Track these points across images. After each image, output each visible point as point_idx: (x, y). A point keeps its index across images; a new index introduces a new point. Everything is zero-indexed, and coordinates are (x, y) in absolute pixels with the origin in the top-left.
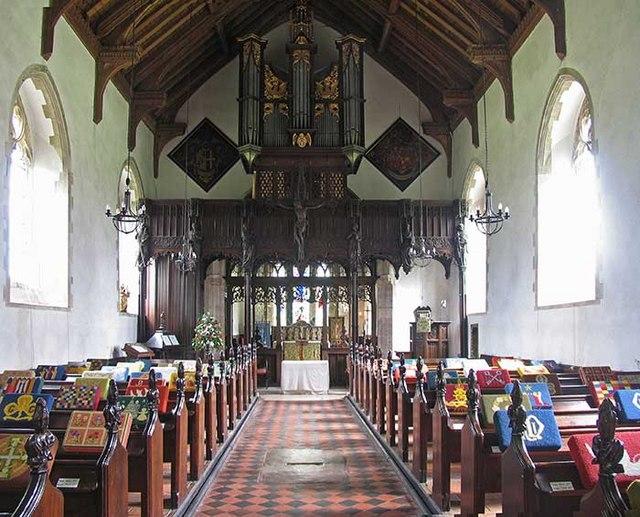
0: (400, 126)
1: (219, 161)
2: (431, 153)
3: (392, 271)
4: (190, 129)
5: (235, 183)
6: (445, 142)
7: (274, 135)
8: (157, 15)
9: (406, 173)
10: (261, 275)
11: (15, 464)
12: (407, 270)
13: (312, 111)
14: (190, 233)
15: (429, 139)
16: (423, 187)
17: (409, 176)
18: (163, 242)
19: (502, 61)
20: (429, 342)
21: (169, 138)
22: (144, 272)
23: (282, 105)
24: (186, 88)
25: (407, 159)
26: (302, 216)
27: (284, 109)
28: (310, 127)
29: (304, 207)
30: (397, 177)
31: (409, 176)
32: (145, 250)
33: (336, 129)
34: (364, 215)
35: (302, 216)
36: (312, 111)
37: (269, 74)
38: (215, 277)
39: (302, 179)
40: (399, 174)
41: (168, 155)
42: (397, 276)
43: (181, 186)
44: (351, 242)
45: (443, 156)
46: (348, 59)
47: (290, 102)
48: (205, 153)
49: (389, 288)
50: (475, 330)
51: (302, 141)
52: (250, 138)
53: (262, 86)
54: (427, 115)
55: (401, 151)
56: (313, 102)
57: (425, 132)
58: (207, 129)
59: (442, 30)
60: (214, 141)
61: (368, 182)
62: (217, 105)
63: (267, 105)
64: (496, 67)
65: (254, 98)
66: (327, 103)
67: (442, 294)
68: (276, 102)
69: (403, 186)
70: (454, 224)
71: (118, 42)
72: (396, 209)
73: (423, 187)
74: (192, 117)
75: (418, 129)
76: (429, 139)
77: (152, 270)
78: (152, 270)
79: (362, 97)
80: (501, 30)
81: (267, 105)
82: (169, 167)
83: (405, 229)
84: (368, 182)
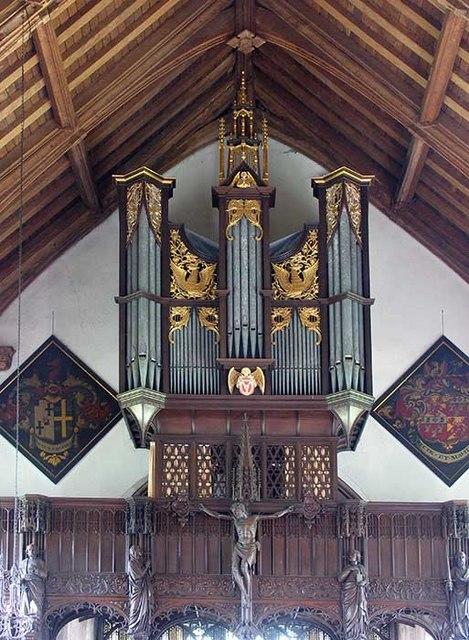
5: (114, 467)
7: (191, 368)
14: (22, 564)
26: (247, 532)
28: (261, 354)
30: (436, 455)
33: (315, 360)
35: (247, 532)
36: (266, 322)
46: (338, 218)
51: (247, 382)
53: (166, 274)
56: (267, 305)
58: (56, 360)
60: (71, 382)
63: (175, 311)
65: (151, 297)
66: (295, 305)
68: (194, 305)
79: (366, 292)
81: (175, 311)
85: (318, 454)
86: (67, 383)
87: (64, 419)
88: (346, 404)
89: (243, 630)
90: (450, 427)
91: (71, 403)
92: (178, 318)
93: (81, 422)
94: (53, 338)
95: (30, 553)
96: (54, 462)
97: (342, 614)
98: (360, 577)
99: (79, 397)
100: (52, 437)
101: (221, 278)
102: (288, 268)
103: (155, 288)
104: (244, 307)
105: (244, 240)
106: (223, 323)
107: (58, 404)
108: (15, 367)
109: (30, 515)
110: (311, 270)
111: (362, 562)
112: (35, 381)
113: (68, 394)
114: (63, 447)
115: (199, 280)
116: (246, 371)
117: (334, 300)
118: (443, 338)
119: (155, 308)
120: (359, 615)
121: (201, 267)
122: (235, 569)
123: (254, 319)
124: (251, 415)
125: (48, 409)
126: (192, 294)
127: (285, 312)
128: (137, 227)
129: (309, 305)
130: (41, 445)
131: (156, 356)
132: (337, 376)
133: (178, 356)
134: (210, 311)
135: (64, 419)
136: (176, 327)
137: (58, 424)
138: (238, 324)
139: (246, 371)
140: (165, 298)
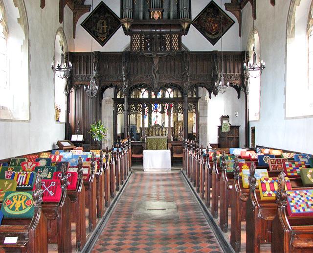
1: (110, 27)
3: (208, 94)
5: (119, 42)
6: (238, 15)
9: (215, 34)
10: (133, 97)
14: (94, 72)
15: (228, 13)
16: (228, 42)
17: (216, 36)
18: (80, 77)
20: (229, 137)
22: (68, 96)
25: (216, 25)
30: (210, 36)
32: (69, 83)
33: (176, 8)
35: (156, 61)
38: (107, 98)
41: (81, 25)
43: (86, 43)
45: (236, 24)
49: (205, 104)
50: (253, 130)
55: (213, 22)
60: (107, 15)
61: (194, 41)
73: (228, 42)
75: (223, 8)
76: (228, 13)
77: (73, 95)
82: (82, 32)
84: (194, 41)
90: (214, 28)
93: (110, 27)
96: (102, 40)
99: (109, 20)
112: (97, 15)
114: (105, 36)
116: (156, 12)
130: (98, 35)
135: (105, 27)
137: (103, 28)
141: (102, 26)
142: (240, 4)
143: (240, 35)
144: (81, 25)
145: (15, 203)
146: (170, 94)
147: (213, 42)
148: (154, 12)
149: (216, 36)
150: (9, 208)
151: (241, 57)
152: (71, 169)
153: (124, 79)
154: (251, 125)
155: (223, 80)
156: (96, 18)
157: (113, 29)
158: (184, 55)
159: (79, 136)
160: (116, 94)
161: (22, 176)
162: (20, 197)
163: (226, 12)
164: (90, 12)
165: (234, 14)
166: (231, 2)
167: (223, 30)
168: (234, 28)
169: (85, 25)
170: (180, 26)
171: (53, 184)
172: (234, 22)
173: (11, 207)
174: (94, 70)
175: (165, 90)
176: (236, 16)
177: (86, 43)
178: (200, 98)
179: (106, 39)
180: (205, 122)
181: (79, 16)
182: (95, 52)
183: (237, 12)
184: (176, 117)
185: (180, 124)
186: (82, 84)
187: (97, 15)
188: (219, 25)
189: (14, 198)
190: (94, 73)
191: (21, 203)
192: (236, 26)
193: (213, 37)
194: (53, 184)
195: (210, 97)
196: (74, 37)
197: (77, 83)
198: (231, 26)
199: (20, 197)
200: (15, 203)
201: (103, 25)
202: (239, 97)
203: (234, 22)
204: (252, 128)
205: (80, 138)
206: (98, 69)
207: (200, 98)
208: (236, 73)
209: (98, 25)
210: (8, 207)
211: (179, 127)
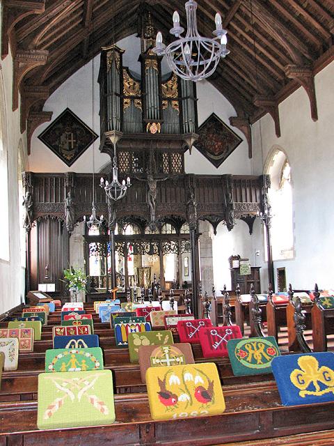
0: (213, 119)
1: (79, 142)
2: (236, 139)
3: (212, 229)
4: (54, 117)
5: (92, 160)
6: (246, 132)
7: (133, 124)
8: (277, 51)
9: (219, 154)
10: (148, 233)
11: (173, 355)
12: (230, 228)
13: (161, 105)
14: (67, 200)
15: (234, 129)
16: (234, 164)
17: (220, 157)
18: (46, 206)
19: (308, 77)
20: (244, 280)
21: (40, 123)
22: (29, 231)
23: (137, 101)
24: (53, 84)
25: (220, 144)
26: (153, 187)
27: (138, 103)
28: (160, 118)
29: (154, 179)
30: (212, 157)
31: (221, 156)
32: (31, 214)
33: (177, 120)
34: (198, 186)
35: (153, 187)
36: (161, 105)
37: (126, 76)
38: (77, 235)
39: (152, 158)
40: (215, 155)
41: (38, 137)
42: (215, 233)
43: (49, 162)
44: (190, 206)
45: (245, 142)
46: (111, 64)
47: (143, 99)
48: (67, 135)
49: (209, 241)
50: (282, 272)
51: (154, 128)
52: (114, 126)
53: (122, 86)
54: (234, 114)
55: (216, 139)
56: (161, 98)
57: (231, 124)
58: (68, 117)
59: (255, 50)
60: (75, 126)
61: (195, 163)
62: (79, 95)
63: (125, 100)
64: (304, 81)
65: (116, 94)
66: (170, 100)
67: (248, 247)
68: (132, 98)
69: (217, 164)
70: (261, 192)
71: (30, 47)
72: (222, 182)
73: (234, 164)
74: (56, 105)
75: (227, 122)
76: (234, 129)
77: (34, 231)
78: (34, 231)
79: (195, 96)
80: (307, 56)
81: (125, 100)
82: (40, 148)
83: (227, 196)
84: (195, 163)
85: (176, 157)
86: (73, 127)
87: (72, 141)
88: (190, 138)
89: (152, 224)
90: (217, 146)
91: (75, 134)
92: (126, 103)
93: (79, 142)
94: (68, 109)
95: (69, 195)
96: (69, 158)
97: (187, 216)
98: (194, 203)
99: (78, 132)
100: (68, 148)
101: (143, 87)
102: (167, 85)
103: (118, 92)
104: (152, 100)
105: (151, 75)
106: (144, 106)
107: (70, 135)
108: (52, 120)
109: (26, 180)
110: (175, 87)
111: (194, 197)
112: (61, 126)
113: (74, 131)
114: (72, 153)
115: (134, 89)
116: (154, 124)
117: (184, 99)
118: (68, 109)
119: (118, 98)
120: (194, 218)
121: (134, 84)
122: (149, 201)
123: (156, 104)
124: (154, 141)
125: (66, 137)
126: (131, 94)
127: (166, 102)
128: (111, 68)
129: (175, 100)
130: (63, 151)
131: (193, 121)
132: (185, 128)
133: (127, 117)
134: (139, 101)
135: (72, 141)
136: (126, 106)
137: (70, 143)
138: (150, 106)
139: (154, 124)
140: (121, 96)
141: (66, 140)
142: (249, 119)
143: (250, 156)
144: (38, 137)
145: (253, 354)
146: (129, 231)
147: (217, 164)
148: (151, 124)
149: (220, 157)
150: (248, 362)
151: (260, 183)
152: (170, 318)
153: (110, 209)
154: (277, 266)
155: (94, 213)
156: (59, 129)
157: (83, 144)
158: (189, 181)
159: (48, 285)
160: (87, 229)
161: (133, 328)
162: (254, 345)
163: (231, 127)
164: (50, 123)
165: (242, 130)
166: (236, 116)
167: (228, 150)
168: (242, 149)
169: (44, 137)
170: (183, 142)
171: (214, 333)
172: (242, 140)
173: (249, 359)
174: (67, 197)
175: (121, 227)
176: (244, 133)
177: (49, 162)
178: (201, 234)
179: (74, 157)
180: (209, 265)
181: (36, 126)
182: (69, 173)
183: (245, 128)
184: (138, 261)
185: (146, 270)
186: (49, 216)
187: (61, 126)
188: (223, 144)
189: (246, 346)
190: (67, 202)
191: (261, 353)
192: (243, 146)
193: (216, 158)
194: (214, 333)
195: (215, 233)
196: (29, 154)
197: (42, 214)
198: (239, 144)
199: (254, 345)
200: (253, 354)
201: (70, 139)
202: (251, 232)
203: (242, 140)
204: (278, 269)
205: (51, 288)
206: (73, 196)
207: (201, 234)
208: (254, 202)
209: (63, 138)
210: (245, 359)
211: (145, 275)
